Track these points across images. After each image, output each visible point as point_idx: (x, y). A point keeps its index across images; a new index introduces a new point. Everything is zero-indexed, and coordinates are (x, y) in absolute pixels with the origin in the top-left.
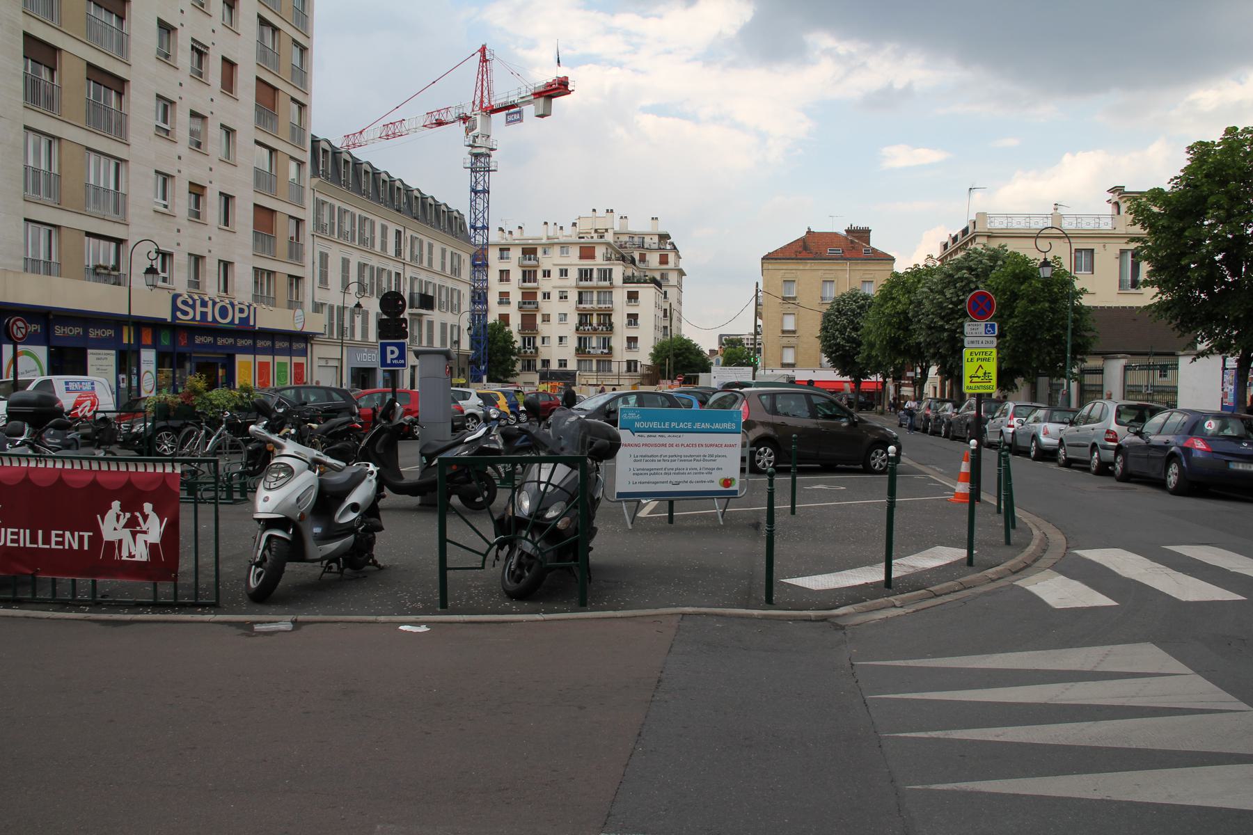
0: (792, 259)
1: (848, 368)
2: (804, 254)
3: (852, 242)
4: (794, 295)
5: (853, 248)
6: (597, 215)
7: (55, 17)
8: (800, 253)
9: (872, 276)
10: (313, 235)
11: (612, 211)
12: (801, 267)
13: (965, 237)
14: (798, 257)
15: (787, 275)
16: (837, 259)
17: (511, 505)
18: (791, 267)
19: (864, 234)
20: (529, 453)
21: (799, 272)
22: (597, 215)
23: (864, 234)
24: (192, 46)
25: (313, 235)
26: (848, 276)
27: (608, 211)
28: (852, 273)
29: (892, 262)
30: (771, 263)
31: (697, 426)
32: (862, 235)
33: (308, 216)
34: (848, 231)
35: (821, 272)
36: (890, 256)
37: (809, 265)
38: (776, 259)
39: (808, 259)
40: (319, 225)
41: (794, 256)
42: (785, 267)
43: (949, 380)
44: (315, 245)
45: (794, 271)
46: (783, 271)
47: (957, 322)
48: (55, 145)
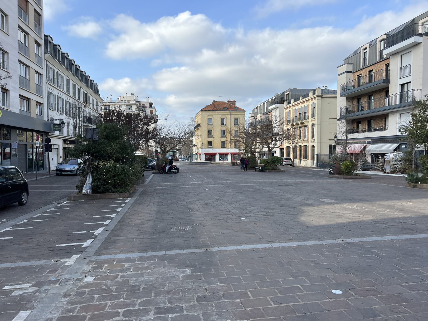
6: (128, 95)
7: (40, 64)
8: (213, 108)
10: (47, 83)
11: (133, 94)
12: (214, 113)
13: (287, 106)
14: (213, 110)
16: (312, 132)
19: (234, 102)
21: (213, 115)
22: (128, 95)
23: (234, 102)
24: (254, 109)
25: (47, 83)
27: (132, 94)
32: (233, 102)
33: (44, 101)
34: (228, 101)
37: (217, 113)
38: (205, 110)
40: (49, 106)
41: (212, 110)
42: (208, 113)
44: (48, 88)
48: (27, 69)
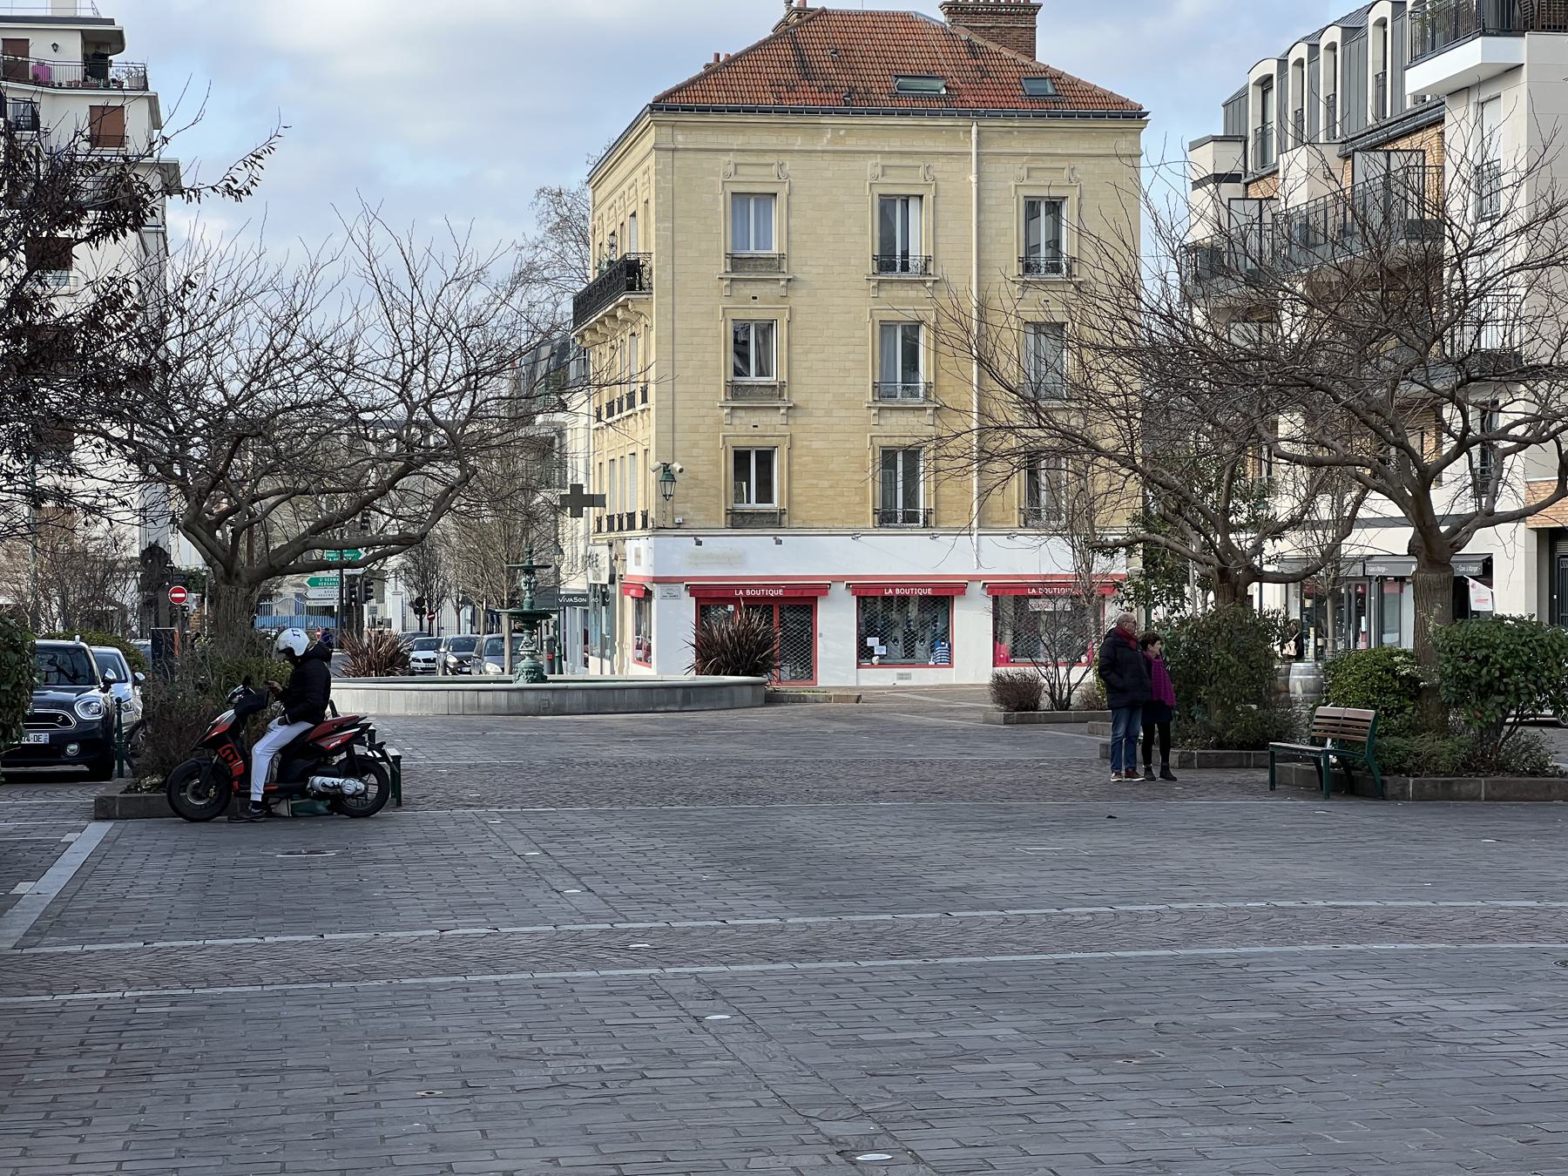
0: (767, 111)
1: (138, 642)
2: (806, 95)
3: (972, 48)
4: (775, 250)
5: (984, 73)
9: (1058, 179)
12: (798, 142)
14: (787, 104)
15: (893, 177)
17: (799, 820)
18: (757, 140)
20: (324, 785)
26: (973, 179)
28: (993, 168)
29: (1134, 124)
30: (685, 127)
31: (669, 708)
32: (1003, 22)
35: (725, 158)
36: (1124, 102)
37: (832, 132)
39: (826, 113)
41: (771, 101)
43: (323, 744)
45: (768, 159)
46: (731, 157)
47: (131, 434)
